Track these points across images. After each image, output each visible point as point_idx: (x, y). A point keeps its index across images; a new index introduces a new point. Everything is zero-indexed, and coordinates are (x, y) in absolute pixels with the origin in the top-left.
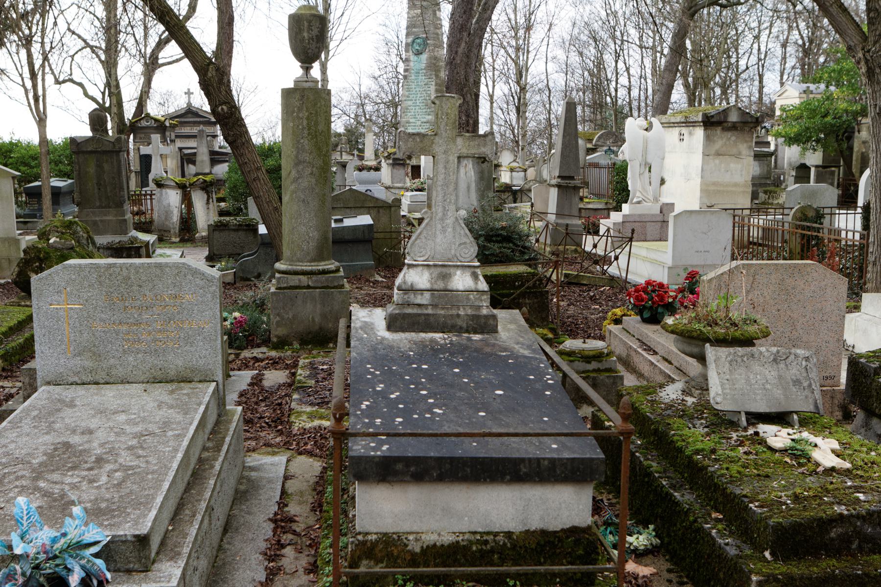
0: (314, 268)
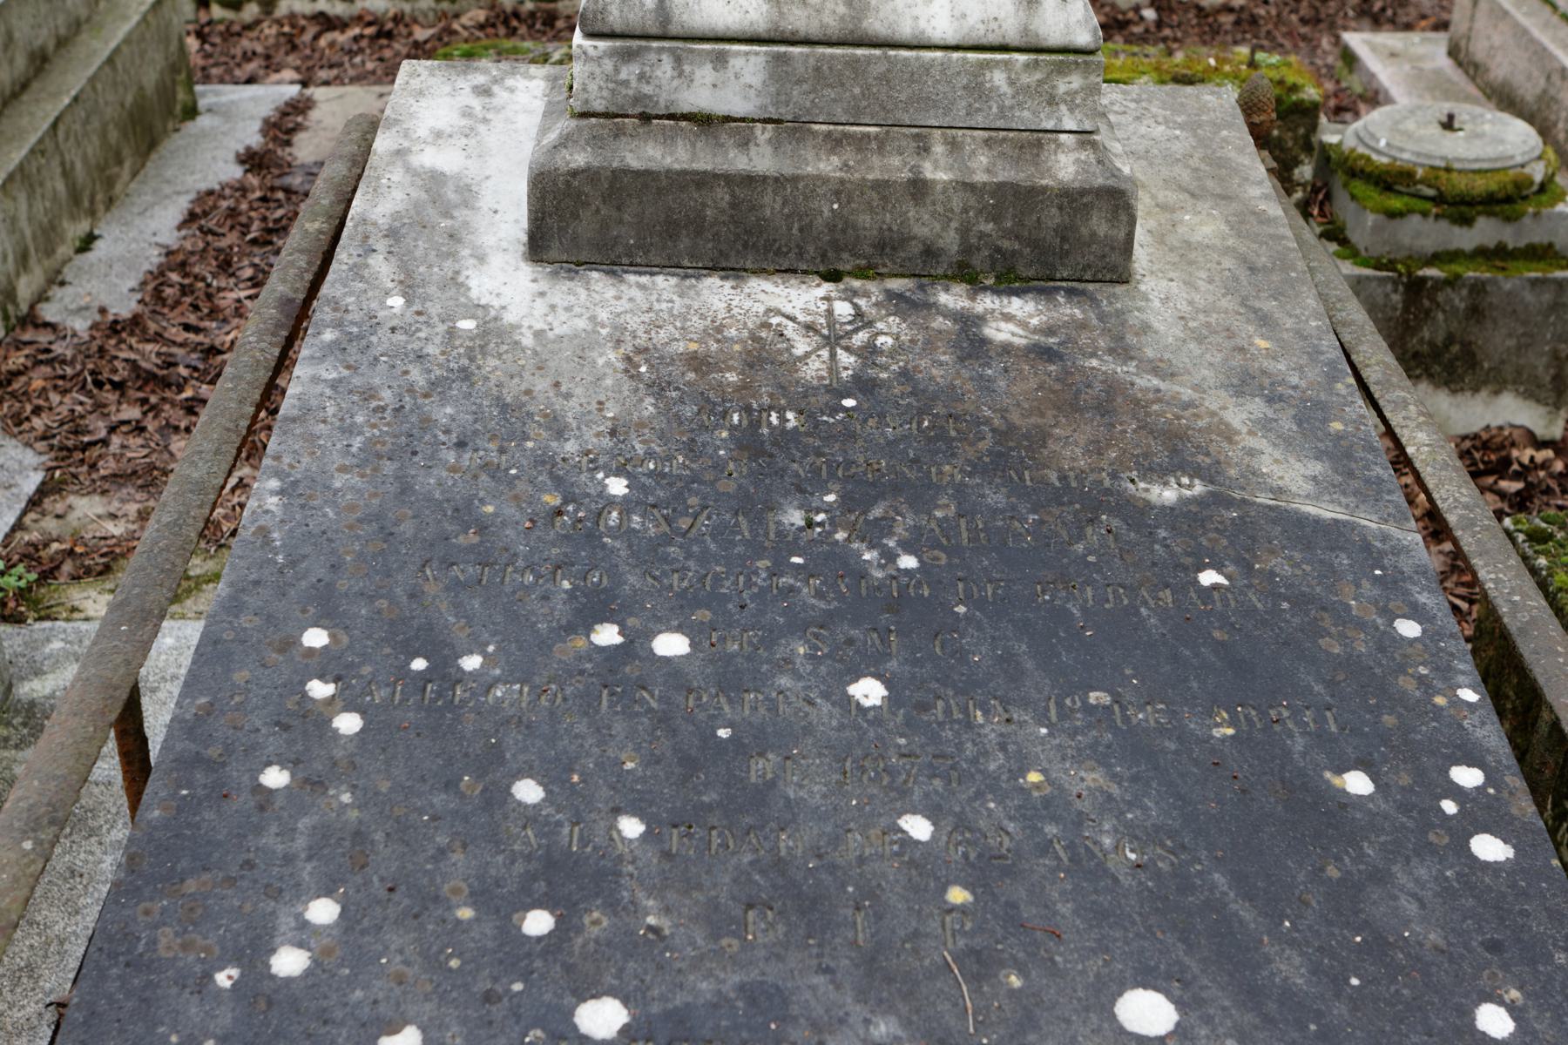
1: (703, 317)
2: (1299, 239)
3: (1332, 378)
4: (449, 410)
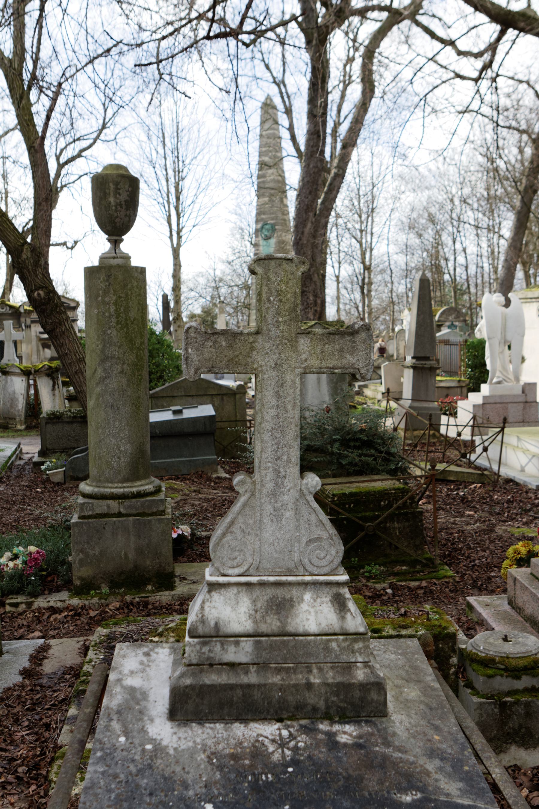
0: (126, 490)
1: (234, 739)
2: (447, 697)
3: (463, 749)
4: (145, 781)
